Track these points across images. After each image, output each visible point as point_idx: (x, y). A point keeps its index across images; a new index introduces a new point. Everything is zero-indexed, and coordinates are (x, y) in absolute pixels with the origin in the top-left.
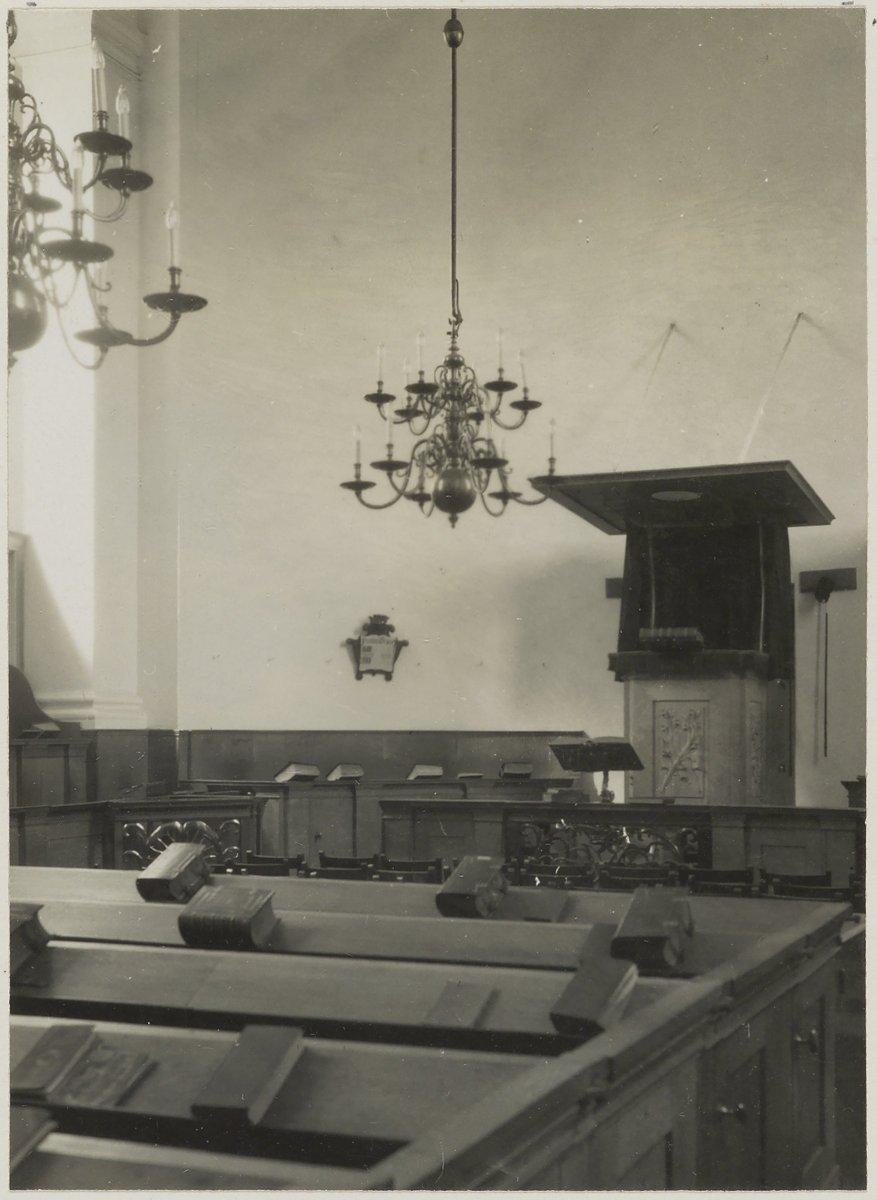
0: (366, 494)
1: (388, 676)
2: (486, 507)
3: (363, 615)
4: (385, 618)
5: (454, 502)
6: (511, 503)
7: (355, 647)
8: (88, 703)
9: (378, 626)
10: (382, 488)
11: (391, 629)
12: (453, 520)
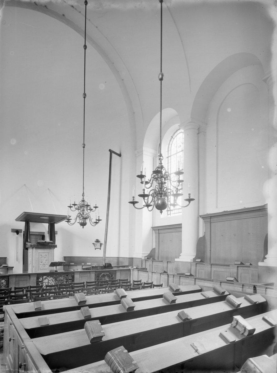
0: (136, 205)
10: (142, 202)
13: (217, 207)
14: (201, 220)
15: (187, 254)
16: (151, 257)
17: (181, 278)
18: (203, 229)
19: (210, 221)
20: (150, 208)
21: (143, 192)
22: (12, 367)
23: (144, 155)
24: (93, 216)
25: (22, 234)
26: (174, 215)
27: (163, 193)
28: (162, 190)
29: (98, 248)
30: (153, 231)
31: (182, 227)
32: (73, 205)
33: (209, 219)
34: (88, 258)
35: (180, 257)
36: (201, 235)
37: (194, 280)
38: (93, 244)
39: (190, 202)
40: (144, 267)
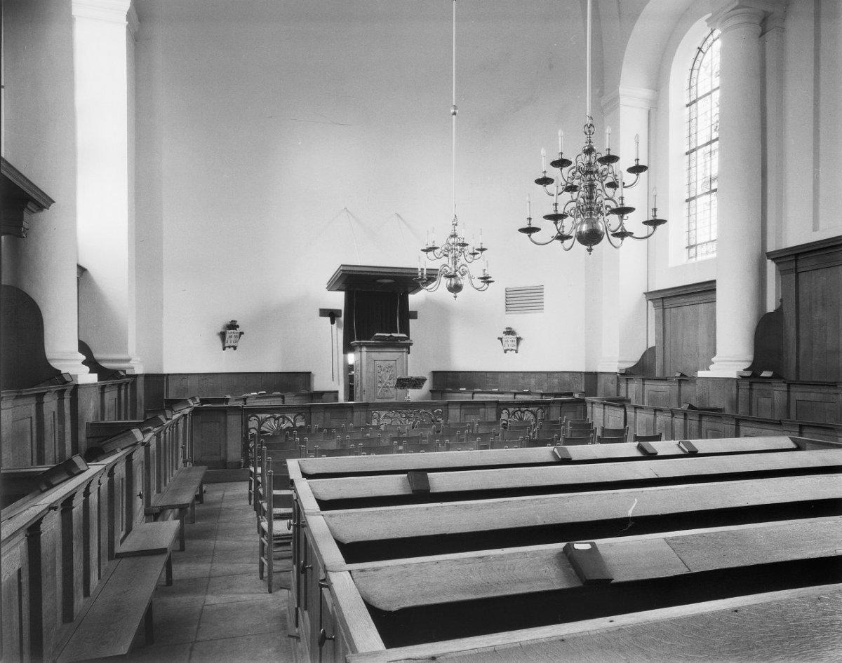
0: (534, 235)
1: (235, 348)
2: (611, 243)
3: (228, 320)
4: (235, 322)
5: (591, 238)
6: (627, 239)
7: (223, 335)
8: (128, 360)
9: (233, 326)
10: (549, 229)
11: (238, 326)
12: (590, 250)
13: (815, 229)
14: (771, 266)
15: (730, 356)
16: (642, 370)
17: (704, 419)
18: (777, 293)
19: (796, 269)
20: (568, 243)
21: (554, 208)
22: (343, 639)
23: (622, 108)
24: (475, 268)
25: (342, 319)
26: (704, 257)
27: (595, 207)
28: (594, 201)
29: (512, 350)
30: (650, 302)
31: (715, 289)
32: (478, 250)
33: (794, 261)
34: (488, 375)
35: (711, 367)
36: (771, 307)
37: (734, 422)
38: (499, 339)
39: (655, 228)
40: (623, 394)
